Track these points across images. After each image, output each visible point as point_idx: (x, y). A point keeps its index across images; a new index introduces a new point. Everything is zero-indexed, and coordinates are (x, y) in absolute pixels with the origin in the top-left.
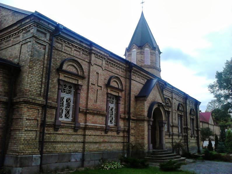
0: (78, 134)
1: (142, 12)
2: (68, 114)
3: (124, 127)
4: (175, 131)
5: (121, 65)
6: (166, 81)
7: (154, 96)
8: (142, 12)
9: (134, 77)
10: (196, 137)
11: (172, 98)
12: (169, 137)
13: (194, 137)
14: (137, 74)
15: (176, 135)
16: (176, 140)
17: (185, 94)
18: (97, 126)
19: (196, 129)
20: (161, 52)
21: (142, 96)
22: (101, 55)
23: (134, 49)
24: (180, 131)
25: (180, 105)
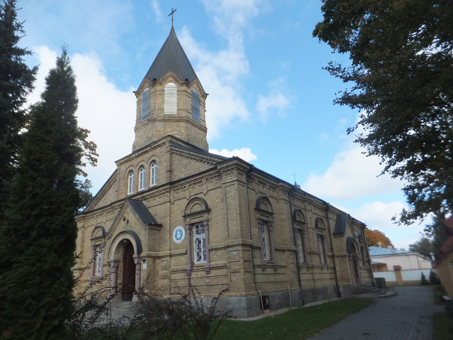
0: (277, 273)
1: (173, 27)
2: (197, 252)
3: (114, 257)
4: (315, 261)
5: (197, 156)
6: (136, 111)
7: (348, 233)
8: (173, 27)
9: (331, 216)
10: (331, 268)
11: (305, 209)
12: (308, 271)
13: (328, 268)
14: (296, 197)
15: (317, 267)
16: (89, 291)
17: (324, 203)
18: (218, 264)
19: (329, 253)
20: (206, 92)
21: (339, 233)
22: (191, 155)
23: (146, 88)
24: (323, 261)
25: (297, 213)
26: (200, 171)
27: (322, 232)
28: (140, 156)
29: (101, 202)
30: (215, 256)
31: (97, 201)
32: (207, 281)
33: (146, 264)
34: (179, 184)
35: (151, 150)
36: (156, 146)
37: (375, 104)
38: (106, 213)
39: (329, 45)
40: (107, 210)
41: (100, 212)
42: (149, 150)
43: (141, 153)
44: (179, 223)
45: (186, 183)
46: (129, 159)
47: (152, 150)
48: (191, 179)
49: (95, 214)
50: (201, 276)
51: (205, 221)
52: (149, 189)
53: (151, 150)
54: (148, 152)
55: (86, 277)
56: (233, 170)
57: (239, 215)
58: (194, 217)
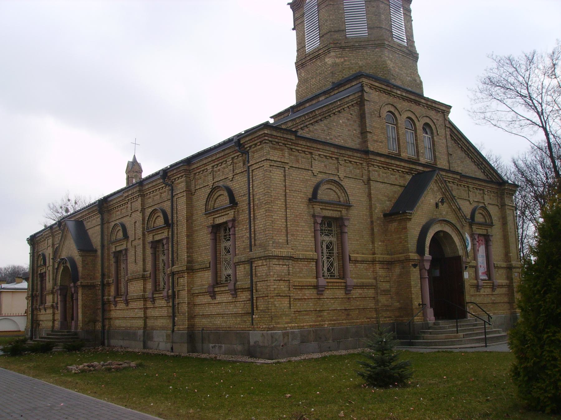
26: (475, 175)
27: (178, 291)
28: (406, 100)
29: (317, 127)
30: (497, 274)
31: (311, 120)
32: (493, 299)
33: (438, 270)
34: (465, 180)
35: (425, 105)
36: (432, 106)
37: (549, 190)
38: (345, 160)
39: (289, 6)
40: (349, 156)
41: (333, 153)
42: (423, 103)
43: (411, 98)
44: (293, 216)
45: (323, 149)
46: (390, 91)
47: (425, 107)
48: (477, 182)
49: (318, 149)
50: (487, 293)
51: (229, 221)
52: (427, 164)
53: (425, 105)
54: (419, 105)
55: (301, 278)
56: (262, 143)
57: (185, 221)
58: (480, 228)
